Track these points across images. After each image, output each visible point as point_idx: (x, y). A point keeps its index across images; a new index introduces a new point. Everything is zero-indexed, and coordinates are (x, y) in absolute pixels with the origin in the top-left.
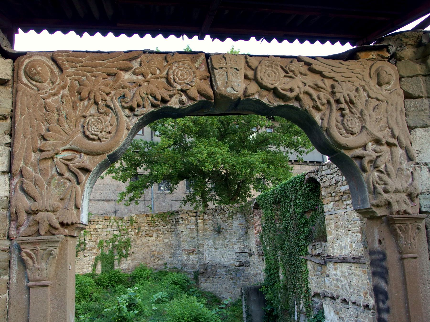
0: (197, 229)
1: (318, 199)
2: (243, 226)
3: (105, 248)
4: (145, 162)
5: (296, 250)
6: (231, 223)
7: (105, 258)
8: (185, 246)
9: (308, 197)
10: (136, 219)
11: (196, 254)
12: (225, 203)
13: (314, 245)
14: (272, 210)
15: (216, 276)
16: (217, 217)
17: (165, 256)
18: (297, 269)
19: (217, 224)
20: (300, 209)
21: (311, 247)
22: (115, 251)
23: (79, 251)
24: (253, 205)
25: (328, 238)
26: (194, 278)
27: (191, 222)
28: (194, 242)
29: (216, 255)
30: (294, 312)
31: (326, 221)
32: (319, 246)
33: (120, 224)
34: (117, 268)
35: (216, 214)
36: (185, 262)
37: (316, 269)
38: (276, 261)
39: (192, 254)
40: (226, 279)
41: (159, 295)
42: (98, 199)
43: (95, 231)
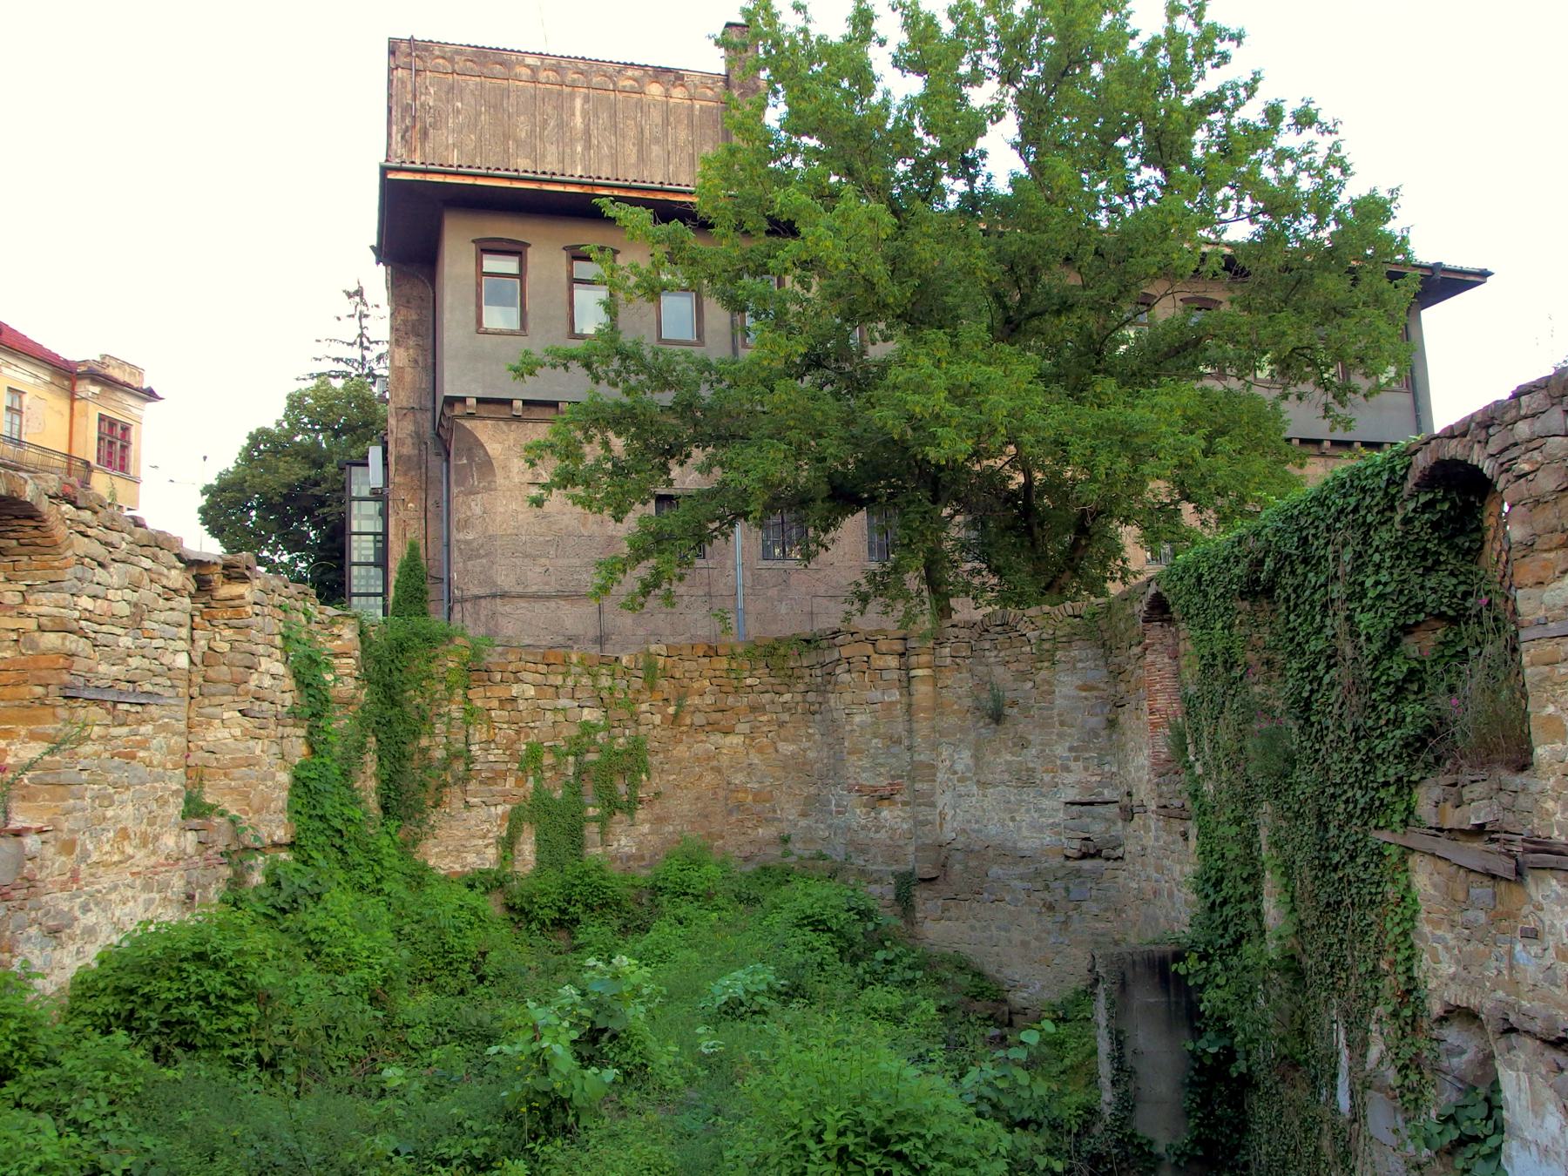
0: (910, 705)
1: (1474, 568)
2: (1095, 693)
3: (548, 774)
4: (701, 441)
5: (1356, 802)
6: (1048, 682)
7: (549, 813)
8: (860, 770)
9: (1424, 558)
10: (669, 666)
11: (905, 804)
12: (1021, 601)
13: (1454, 785)
14: (1230, 627)
15: (986, 895)
16: (991, 656)
17: (782, 810)
18: (1354, 891)
19: (988, 687)
20: (1383, 615)
21: (1437, 793)
22: (588, 788)
23: (446, 785)
24: (1141, 607)
25: (1541, 752)
26: (898, 898)
27: (885, 677)
28: (895, 756)
29: (984, 811)
30: (1335, 1076)
31: (1528, 671)
32: (1479, 789)
33: (605, 682)
34: (594, 851)
35: (987, 645)
36: (862, 834)
37: (1461, 896)
38: (1250, 845)
39: (886, 802)
40: (1027, 909)
41: (734, 983)
42: (534, 588)
43: (509, 707)
